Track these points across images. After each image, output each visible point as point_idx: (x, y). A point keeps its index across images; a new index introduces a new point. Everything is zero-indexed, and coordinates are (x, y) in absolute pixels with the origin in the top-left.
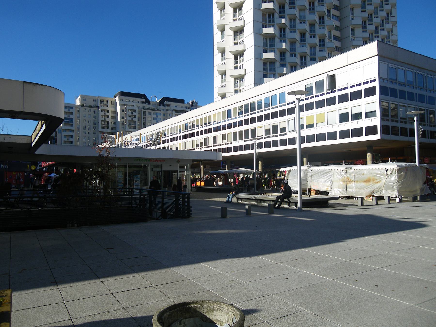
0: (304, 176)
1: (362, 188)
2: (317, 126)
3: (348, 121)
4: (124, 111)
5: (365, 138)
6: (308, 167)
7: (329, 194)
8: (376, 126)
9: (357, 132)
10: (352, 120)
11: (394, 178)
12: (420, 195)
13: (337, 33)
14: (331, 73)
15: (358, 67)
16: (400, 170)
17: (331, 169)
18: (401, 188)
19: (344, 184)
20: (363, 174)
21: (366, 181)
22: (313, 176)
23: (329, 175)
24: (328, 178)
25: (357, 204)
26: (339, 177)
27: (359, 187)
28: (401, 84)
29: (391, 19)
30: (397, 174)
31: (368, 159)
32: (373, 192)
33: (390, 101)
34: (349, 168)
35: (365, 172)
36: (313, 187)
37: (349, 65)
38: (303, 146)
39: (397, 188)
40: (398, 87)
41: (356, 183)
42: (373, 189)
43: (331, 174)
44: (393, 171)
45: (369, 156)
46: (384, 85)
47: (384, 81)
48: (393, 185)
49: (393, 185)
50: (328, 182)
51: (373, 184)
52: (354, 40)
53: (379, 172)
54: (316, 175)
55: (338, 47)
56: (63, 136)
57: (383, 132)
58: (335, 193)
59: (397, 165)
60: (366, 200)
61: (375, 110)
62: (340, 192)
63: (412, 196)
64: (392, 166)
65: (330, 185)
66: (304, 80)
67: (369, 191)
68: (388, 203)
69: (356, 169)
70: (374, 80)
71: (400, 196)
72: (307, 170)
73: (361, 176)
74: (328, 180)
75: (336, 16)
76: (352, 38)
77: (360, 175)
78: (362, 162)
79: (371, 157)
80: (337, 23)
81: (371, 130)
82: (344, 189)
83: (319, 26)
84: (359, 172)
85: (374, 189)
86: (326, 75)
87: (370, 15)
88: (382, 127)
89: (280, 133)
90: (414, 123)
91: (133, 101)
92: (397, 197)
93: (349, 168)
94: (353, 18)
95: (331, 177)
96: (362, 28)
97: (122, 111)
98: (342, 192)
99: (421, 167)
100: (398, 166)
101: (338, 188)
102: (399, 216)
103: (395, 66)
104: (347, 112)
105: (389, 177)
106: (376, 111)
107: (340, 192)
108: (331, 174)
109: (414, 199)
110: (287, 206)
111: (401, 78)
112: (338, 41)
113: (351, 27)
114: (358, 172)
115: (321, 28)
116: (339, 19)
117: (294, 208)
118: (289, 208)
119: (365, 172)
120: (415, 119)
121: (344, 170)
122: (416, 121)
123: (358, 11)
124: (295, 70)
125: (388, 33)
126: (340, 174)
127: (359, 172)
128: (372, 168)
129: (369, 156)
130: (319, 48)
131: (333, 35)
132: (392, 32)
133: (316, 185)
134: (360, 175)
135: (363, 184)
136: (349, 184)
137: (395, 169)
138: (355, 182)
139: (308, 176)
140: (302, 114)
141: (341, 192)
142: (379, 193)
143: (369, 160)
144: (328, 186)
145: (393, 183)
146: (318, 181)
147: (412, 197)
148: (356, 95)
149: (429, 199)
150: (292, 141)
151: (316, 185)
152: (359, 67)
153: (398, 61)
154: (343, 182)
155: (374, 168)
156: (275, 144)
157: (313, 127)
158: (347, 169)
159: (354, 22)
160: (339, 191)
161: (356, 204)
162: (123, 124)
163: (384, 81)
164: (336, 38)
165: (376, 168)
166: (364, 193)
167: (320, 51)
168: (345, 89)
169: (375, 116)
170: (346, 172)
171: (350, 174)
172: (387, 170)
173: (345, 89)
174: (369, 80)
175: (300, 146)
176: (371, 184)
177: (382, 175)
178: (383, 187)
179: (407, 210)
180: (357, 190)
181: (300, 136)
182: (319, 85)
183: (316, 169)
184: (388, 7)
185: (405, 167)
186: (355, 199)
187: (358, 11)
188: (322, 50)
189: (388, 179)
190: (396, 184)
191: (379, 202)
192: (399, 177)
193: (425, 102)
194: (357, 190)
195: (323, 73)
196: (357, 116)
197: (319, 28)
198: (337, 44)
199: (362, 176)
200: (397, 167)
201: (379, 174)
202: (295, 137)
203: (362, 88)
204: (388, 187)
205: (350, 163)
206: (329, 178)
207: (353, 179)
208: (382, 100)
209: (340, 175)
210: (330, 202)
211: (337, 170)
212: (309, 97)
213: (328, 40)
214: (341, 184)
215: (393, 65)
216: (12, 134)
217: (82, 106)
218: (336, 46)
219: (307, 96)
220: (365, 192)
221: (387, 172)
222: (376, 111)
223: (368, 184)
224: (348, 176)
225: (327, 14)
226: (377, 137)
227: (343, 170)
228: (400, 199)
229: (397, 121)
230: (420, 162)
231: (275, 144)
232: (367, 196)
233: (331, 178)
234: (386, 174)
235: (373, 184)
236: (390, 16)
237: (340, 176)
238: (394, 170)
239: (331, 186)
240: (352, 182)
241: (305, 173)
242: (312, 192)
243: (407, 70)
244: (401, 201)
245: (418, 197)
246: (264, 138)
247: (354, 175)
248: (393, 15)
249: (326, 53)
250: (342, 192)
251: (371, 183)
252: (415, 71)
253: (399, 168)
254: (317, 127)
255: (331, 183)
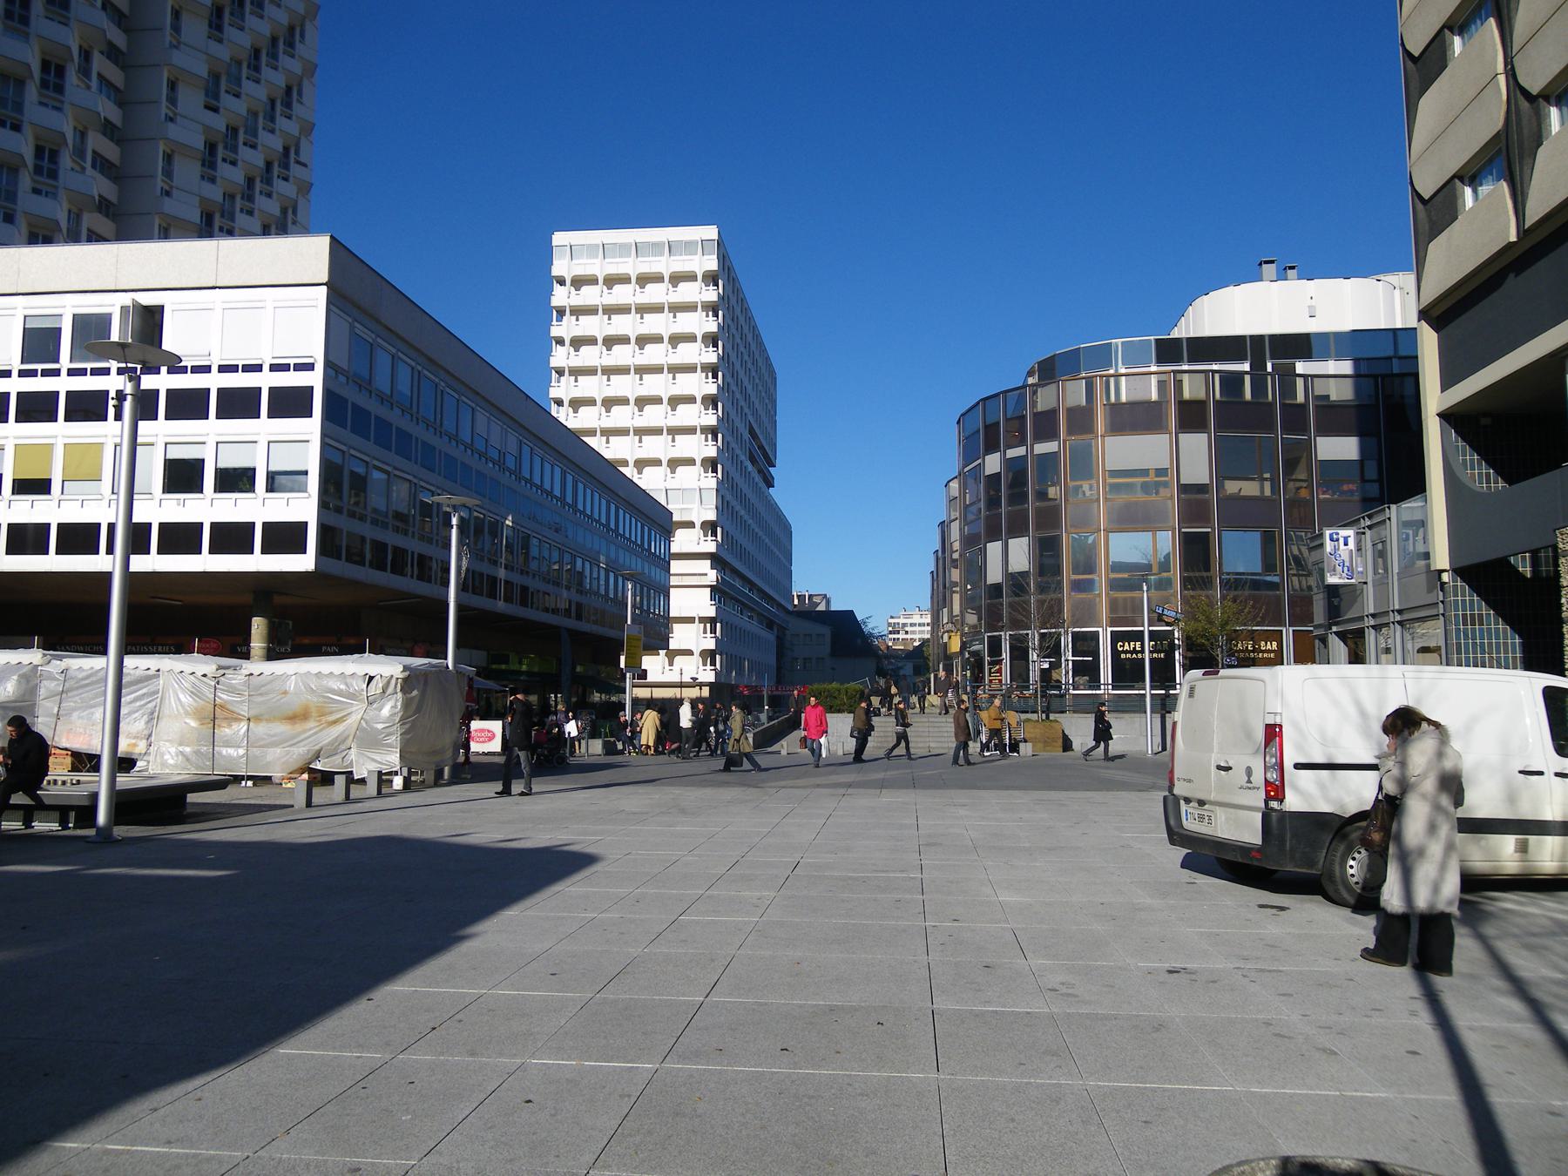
0: (24, 695)
1: (274, 744)
2: (62, 493)
3: (201, 491)
5: (257, 562)
6: (45, 655)
7: (136, 769)
8: (303, 526)
9: (232, 537)
10: (215, 492)
11: (390, 708)
12: (451, 763)
13: (111, 151)
14: (147, 299)
15: (292, 304)
16: (411, 681)
17: (154, 668)
18: (408, 740)
19: (205, 726)
20: (285, 693)
21: (293, 718)
22: (69, 694)
23: (144, 691)
24: (138, 704)
25: (291, 803)
26: (186, 699)
27: (264, 739)
28: (382, 399)
29: (295, 170)
30: (400, 695)
31: (252, 637)
32: (317, 756)
33: (351, 447)
34: (228, 668)
35: (291, 685)
36: (64, 740)
37: (220, 288)
38: (139, 563)
39: (399, 742)
40: (373, 406)
41: (251, 723)
42: (317, 748)
43: (152, 688)
44: (388, 683)
45: (258, 625)
46: (337, 390)
47: (337, 377)
48: (388, 730)
49: (388, 730)
50: (135, 720)
51: (317, 729)
52: (168, 194)
53: (343, 687)
54: (80, 691)
55: (109, 202)
57: (322, 550)
58: (164, 764)
59: (404, 667)
60: (284, 785)
61: (304, 469)
62: (188, 760)
63: (433, 767)
64: (390, 668)
65: (147, 732)
66: (117, 291)
67: (302, 753)
68: (374, 792)
69: (256, 673)
70: (310, 367)
71: (406, 769)
72: (40, 668)
73: (274, 700)
74: (141, 712)
75: (110, 84)
76: (162, 184)
77: (271, 696)
78: (215, 645)
79: (265, 632)
80: (108, 109)
81: (284, 537)
82: (205, 748)
83: (41, 94)
84: (268, 683)
85: (320, 745)
86: (126, 299)
87: (233, 131)
88: (323, 529)
90: (450, 531)
92: (396, 773)
93: (228, 668)
94: (171, 115)
95: (150, 702)
96: (200, 163)
98: (193, 758)
99: (458, 672)
100: (406, 668)
101: (180, 745)
102: (479, 833)
103: (370, 337)
104: (200, 457)
105: (375, 706)
106: (306, 473)
107: (188, 760)
108: (152, 688)
109: (438, 781)
110: (55, 826)
111: (382, 382)
112: (109, 178)
113: (162, 147)
114: (263, 686)
115: (46, 105)
116: (121, 98)
117: (53, 831)
118: (61, 833)
119: (290, 684)
120: (454, 521)
121: (209, 675)
122: (455, 527)
123: (191, 100)
124: (48, 240)
125: (284, 211)
126: (193, 690)
127: (268, 683)
128: (320, 672)
129: (258, 625)
130: (34, 181)
131: (94, 152)
132: (295, 212)
133: (81, 730)
134: (271, 696)
135: (282, 728)
136: (226, 730)
137: (395, 676)
138: (249, 719)
139: (43, 692)
140: (144, 426)
141: (190, 757)
142: (337, 759)
143: (257, 644)
144: (135, 738)
145: (387, 725)
146: (92, 714)
147: (433, 772)
148: (239, 404)
149: (469, 776)
150: (79, 538)
151: (81, 730)
152: (259, 305)
153: (378, 321)
154: (201, 719)
155: (323, 672)
157: (48, 492)
158: (222, 672)
159: (173, 131)
160: (180, 757)
161: (286, 803)
163: (337, 377)
164: (101, 163)
165: (331, 673)
166: (278, 760)
167: (36, 191)
168: (249, 368)
169: (303, 489)
170: (218, 683)
171: (232, 690)
172: (371, 678)
173: (249, 368)
174: (292, 362)
175: (126, 563)
176: (310, 729)
177: (352, 696)
178: (351, 738)
179: (463, 812)
180: (256, 751)
181: (131, 519)
182: (90, 330)
183: (85, 667)
184: (292, 127)
185: (423, 673)
186: (244, 783)
187: (191, 100)
188: (44, 193)
189: (371, 713)
190: (395, 727)
191: (320, 794)
192: (407, 705)
193: (437, 470)
194: (256, 751)
195: (113, 288)
196: (235, 480)
197: (41, 103)
198: (101, 186)
199: (278, 700)
200: (402, 672)
201: (340, 693)
203: (265, 381)
204: (369, 739)
205: (170, 649)
206: (142, 702)
207: (244, 711)
208: (328, 440)
209: (192, 692)
210: (192, 798)
211: (182, 672)
212: (39, 367)
213: (74, 161)
214: (193, 727)
215: (366, 331)
218: (100, 196)
219: (75, 362)
220: (288, 757)
221: (370, 685)
222: (306, 473)
223: (299, 727)
224: (223, 696)
225: (79, 64)
226: (304, 562)
227: (205, 675)
228: (404, 777)
229: (362, 518)
230: (456, 661)
232: (291, 773)
233: (153, 704)
234: (365, 693)
235: (317, 729)
236: (292, 161)
237: (188, 696)
238: (393, 681)
239: (150, 735)
240: (238, 720)
241: (28, 681)
242: (56, 760)
243: (399, 358)
244: (408, 785)
245: (447, 770)
247: (246, 693)
248: (302, 159)
250: (193, 758)
251: (311, 724)
252: (420, 368)
253: (407, 673)
254: (63, 497)
255: (150, 725)
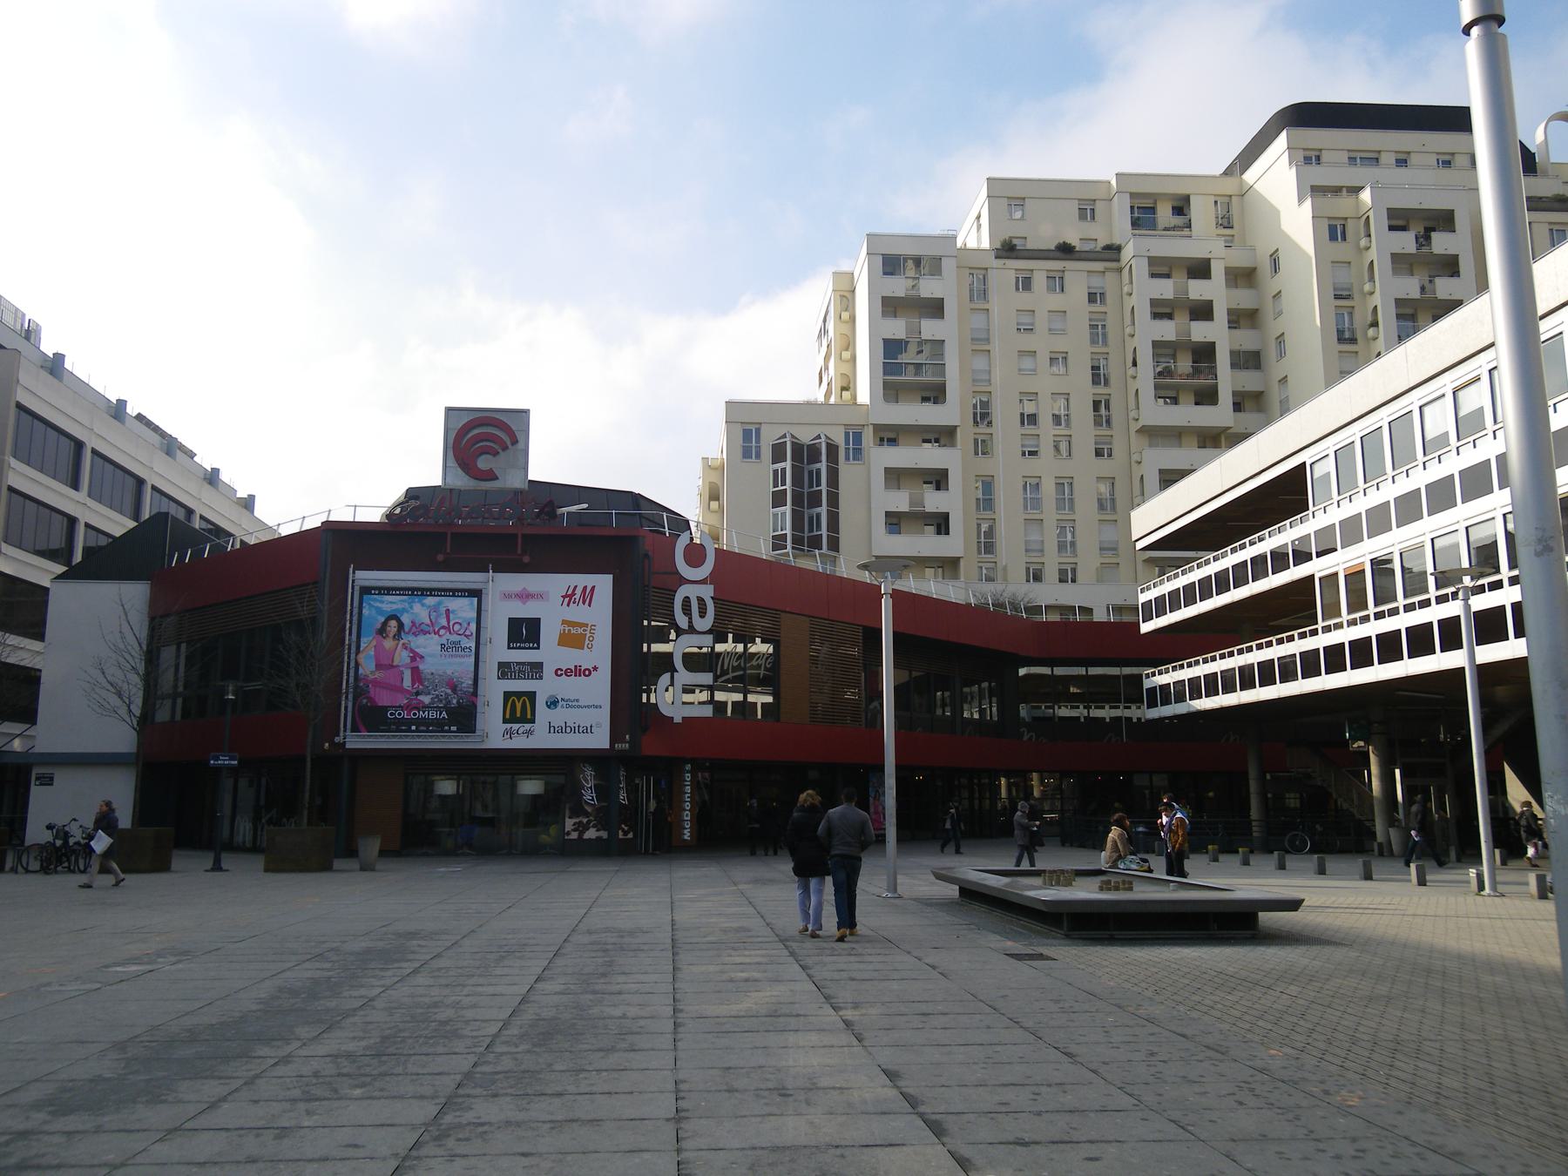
4: (1344, 239)
56: (878, 478)
66: (1224, 492)
89: (1502, 580)
91: (1402, 162)
97: (1333, 237)
156: (1389, 647)
162: (1353, 340)
202: (1432, 622)
216: (480, 663)
217: (1008, 250)
231: (1389, 647)
246: (1401, 609)
249: (1229, 431)
